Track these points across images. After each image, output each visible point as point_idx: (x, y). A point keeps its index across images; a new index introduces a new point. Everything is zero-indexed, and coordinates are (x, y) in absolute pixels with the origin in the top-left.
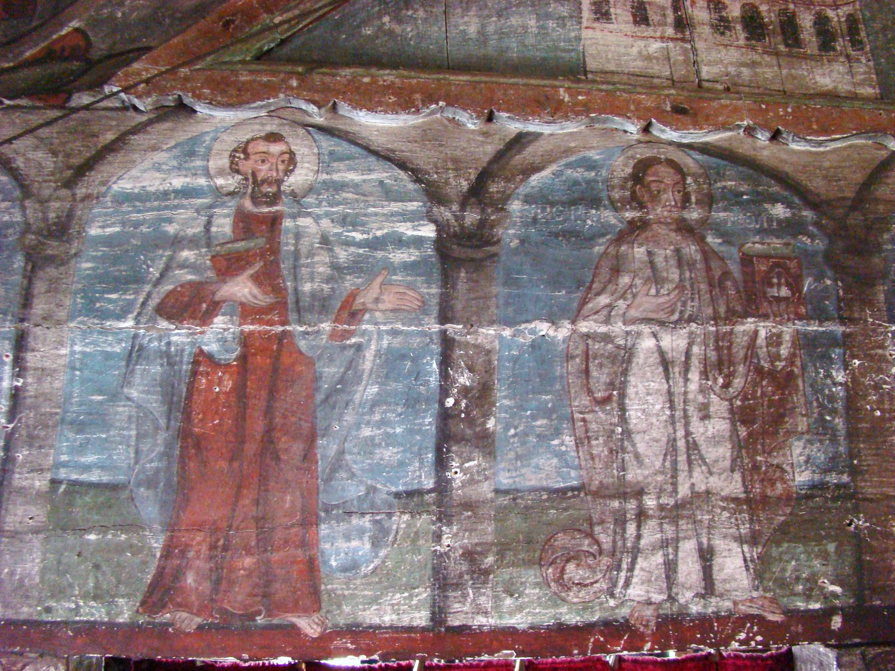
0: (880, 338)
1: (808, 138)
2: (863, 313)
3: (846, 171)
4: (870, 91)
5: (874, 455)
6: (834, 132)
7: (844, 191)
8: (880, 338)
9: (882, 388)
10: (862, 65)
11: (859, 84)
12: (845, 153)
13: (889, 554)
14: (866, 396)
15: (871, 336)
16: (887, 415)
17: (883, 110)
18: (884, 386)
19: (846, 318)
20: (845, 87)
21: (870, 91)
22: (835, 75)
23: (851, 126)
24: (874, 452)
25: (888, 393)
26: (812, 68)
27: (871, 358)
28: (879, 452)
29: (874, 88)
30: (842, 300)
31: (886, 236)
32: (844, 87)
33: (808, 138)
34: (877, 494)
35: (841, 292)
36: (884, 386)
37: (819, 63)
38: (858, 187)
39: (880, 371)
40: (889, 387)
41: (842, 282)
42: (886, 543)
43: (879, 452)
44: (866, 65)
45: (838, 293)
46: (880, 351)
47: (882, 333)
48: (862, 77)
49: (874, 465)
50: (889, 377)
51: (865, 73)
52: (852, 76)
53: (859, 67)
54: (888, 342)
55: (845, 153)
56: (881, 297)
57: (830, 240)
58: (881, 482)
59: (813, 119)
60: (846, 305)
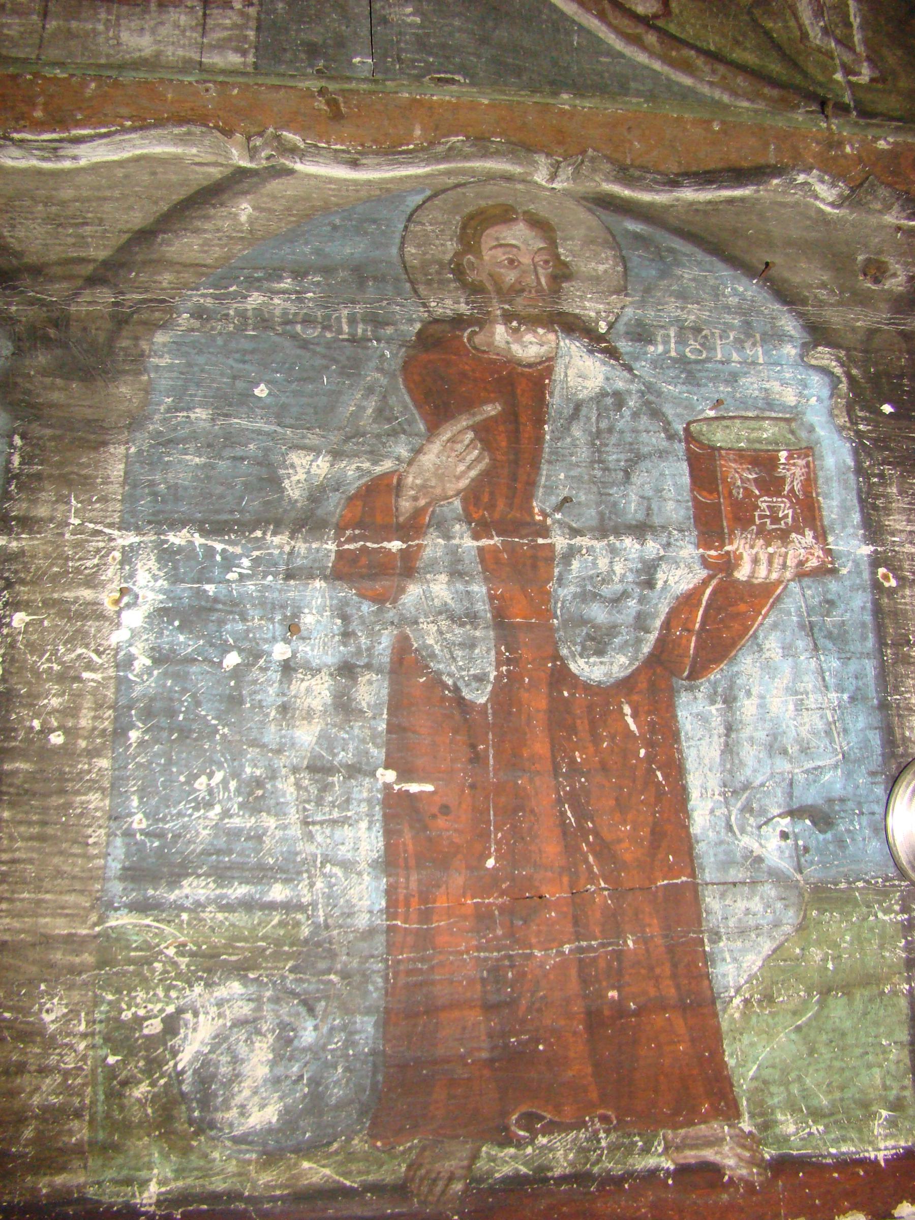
0: (89, 564)
1: (16, 136)
2: (62, 507)
3: (108, 207)
4: (234, 59)
5: (31, 838)
6: (78, 124)
7: (88, 245)
8: (89, 564)
9: (78, 679)
10: (229, 13)
11: (212, 47)
12: (120, 172)
13: (27, 1076)
14: (34, 696)
15: (67, 559)
16: (83, 744)
17: (215, 82)
18: (86, 675)
19: (15, 518)
20: (180, 52)
21: (234, 59)
22: (163, 31)
23: (124, 111)
24: (35, 830)
25: (94, 692)
26: (118, 18)
27: (62, 608)
28: (50, 831)
29: (244, 53)
30: (16, 477)
31: (160, 338)
32: (173, 53)
33: (16, 136)
34: (23, 931)
35: (16, 460)
36: (86, 675)
37: (138, 10)
38: (127, 236)
39: (80, 637)
40: (98, 676)
41: (23, 437)
42: (23, 1052)
43: (50, 831)
44: (242, 14)
45: (9, 462)
46: (87, 594)
47: (98, 551)
48: (226, 34)
49: (31, 861)
50: (99, 653)
51: (235, 26)
52: (203, 35)
53: (225, 17)
54: (110, 573)
55: (120, 172)
56: (117, 470)
57: (19, 348)
58: (39, 902)
59: (41, 100)
60: (20, 488)
